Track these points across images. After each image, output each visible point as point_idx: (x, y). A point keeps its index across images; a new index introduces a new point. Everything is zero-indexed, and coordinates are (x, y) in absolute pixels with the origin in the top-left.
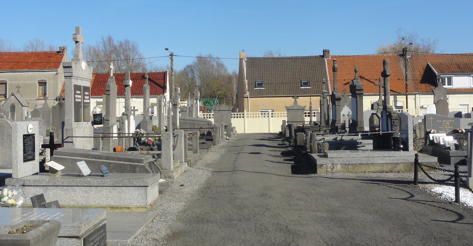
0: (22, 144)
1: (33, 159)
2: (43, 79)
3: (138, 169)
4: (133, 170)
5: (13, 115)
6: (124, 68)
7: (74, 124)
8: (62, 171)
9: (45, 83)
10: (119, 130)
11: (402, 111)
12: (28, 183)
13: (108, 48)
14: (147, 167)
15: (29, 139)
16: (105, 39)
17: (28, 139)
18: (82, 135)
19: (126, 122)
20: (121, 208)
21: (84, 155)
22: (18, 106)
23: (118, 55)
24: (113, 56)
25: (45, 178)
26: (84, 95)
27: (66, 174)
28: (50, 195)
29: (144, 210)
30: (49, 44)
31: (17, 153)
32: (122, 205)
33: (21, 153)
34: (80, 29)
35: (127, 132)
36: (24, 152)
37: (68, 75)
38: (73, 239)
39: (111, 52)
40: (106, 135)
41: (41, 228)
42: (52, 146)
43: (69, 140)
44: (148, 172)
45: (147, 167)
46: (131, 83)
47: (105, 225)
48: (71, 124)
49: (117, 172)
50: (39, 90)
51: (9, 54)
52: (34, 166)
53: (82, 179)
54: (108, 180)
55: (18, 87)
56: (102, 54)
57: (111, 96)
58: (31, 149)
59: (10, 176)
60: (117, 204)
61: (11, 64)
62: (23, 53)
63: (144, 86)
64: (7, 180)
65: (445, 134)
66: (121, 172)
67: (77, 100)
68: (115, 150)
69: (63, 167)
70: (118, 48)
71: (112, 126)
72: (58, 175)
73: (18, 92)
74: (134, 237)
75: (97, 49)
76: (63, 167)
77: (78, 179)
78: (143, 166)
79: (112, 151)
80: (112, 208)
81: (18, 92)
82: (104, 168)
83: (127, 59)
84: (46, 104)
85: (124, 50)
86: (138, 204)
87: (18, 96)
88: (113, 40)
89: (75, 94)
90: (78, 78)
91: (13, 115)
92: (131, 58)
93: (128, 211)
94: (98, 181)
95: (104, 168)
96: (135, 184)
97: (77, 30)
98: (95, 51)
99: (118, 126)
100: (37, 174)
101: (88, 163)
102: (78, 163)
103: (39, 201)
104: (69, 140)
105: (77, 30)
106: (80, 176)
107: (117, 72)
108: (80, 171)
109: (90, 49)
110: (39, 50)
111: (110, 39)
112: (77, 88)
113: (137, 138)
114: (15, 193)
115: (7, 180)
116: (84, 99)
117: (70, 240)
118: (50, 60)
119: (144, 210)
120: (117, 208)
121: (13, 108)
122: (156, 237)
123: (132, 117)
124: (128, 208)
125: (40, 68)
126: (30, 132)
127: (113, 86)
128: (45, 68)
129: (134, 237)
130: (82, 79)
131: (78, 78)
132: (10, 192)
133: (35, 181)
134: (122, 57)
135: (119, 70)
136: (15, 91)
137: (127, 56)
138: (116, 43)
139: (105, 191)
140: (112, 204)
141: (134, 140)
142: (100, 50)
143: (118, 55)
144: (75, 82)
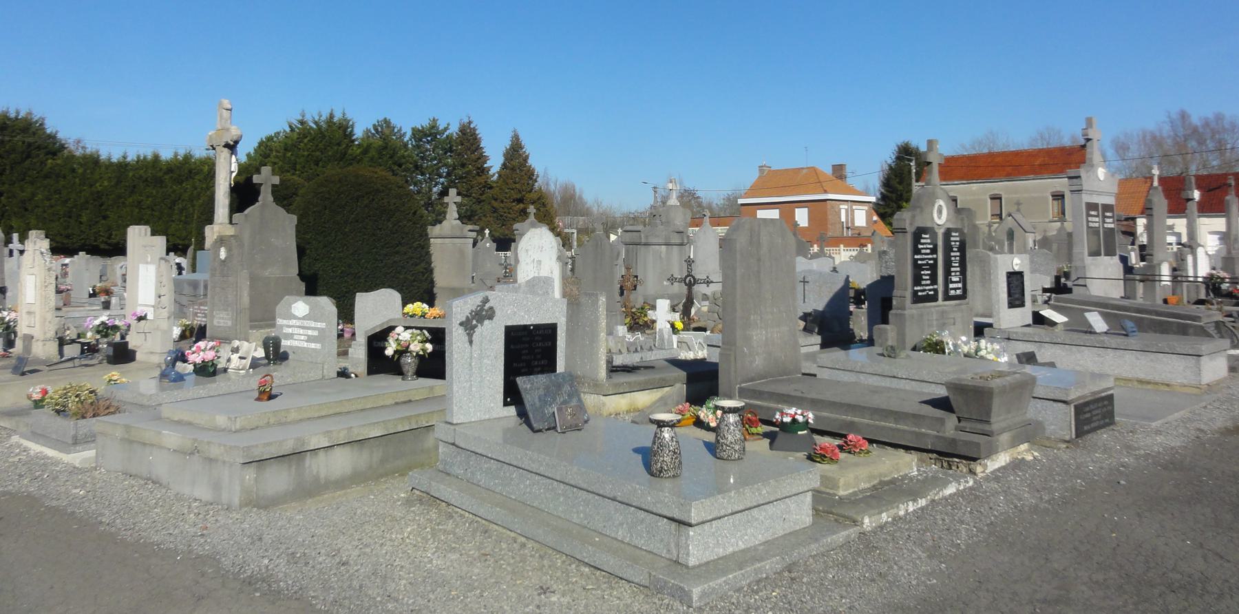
0: (1005, 285)
1: (1022, 305)
2: (1059, 189)
3: (1191, 331)
4: (1183, 330)
5: (1011, 245)
6: (1215, 163)
7: (1089, 260)
8: (1065, 324)
9: (1063, 196)
10: (1174, 270)
11: (608, 255)
12: (1014, 336)
13: (1181, 132)
14: (1212, 330)
15: (1015, 279)
16: (1174, 116)
17: (1014, 278)
18: (1103, 277)
19: (1190, 259)
20: (1157, 384)
21: (1102, 305)
22: (1018, 233)
23: (1201, 142)
24: (1193, 144)
25: (1040, 331)
26: (1105, 217)
27: (1068, 327)
28: (1044, 354)
29: (1196, 391)
30: (1068, 135)
31: (998, 295)
32: (1157, 379)
33: (1004, 296)
34: (1094, 120)
35: (1191, 273)
36: (1010, 294)
37: (1074, 188)
38: (1060, 404)
39: (1186, 138)
40: (1150, 277)
41: (1008, 378)
42: (1059, 288)
43: (1080, 282)
44: (1209, 335)
45: (1212, 330)
46: (1197, 195)
47: (1112, 396)
48: (1083, 260)
49: (1155, 332)
50: (1052, 207)
51: (1003, 154)
52: (1023, 316)
53: (1092, 337)
54: (1132, 341)
55: (1018, 204)
56: (1169, 141)
57: (1155, 217)
58: (1018, 291)
59: (990, 325)
60: (1149, 378)
61: (1009, 169)
62: (1026, 151)
63: (1227, 198)
64: (986, 330)
65: (434, 231)
66: (1162, 333)
67: (1091, 225)
68: (1165, 301)
69: (1065, 319)
70: (1201, 130)
71: (1159, 265)
72: (1058, 329)
73: (1018, 210)
74: (1165, 420)
75: (1158, 134)
76: (1065, 319)
77: (1087, 337)
78: (1202, 327)
79: (1160, 302)
80: (1141, 382)
81: (1018, 210)
82: (1129, 325)
83: (1220, 149)
84: (1062, 229)
85: (1214, 132)
86: (1185, 382)
87: (1018, 217)
88: (1189, 117)
89: (1088, 215)
90: (1092, 192)
91: (1011, 245)
92: (1229, 146)
93: (1167, 389)
94: (1119, 341)
95: (1129, 325)
96: (1179, 350)
97: (1089, 122)
98: (1154, 138)
99: (1170, 264)
100: (1028, 326)
101: (1105, 316)
102: (1087, 314)
103: (1029, 358)
104: (1080, 282)
105: (1089, 122)
106: (1091, 333)
107: (1200, 173)
108: (1090, 326)
109: (1144, 137)
110: (1054, 144)
111: (1184, 116)
112: (1091, 206)
113: (1212, 284)
114: (997, 346)
115: (986, 330)
116: (1104, 222)
117: (1055, 404)
118: (1067, 159)
119: (1196, 391)
120: (1149, 383)
121: (1011, 235)
122: (1202, 427)
123: (1200, 251)
124: (1168, 385)
125: (1053, 172)
126: (1017, 269)
127: (1160, 202)
128: (991, 177)
129: (1165, 420)
130: (1100, 193)
131: (1092, 192)
132: (989, 345)
133: (1025, 334)
134: (1211, 145)
135: (1204, 167)
136: (1013, 209)
137: (1220, 141)
138: (1195, 120)
139: (1129, 356)
140: (1142, 376)
141: (1207, 288)
142: (1165, 135)
143: (1201, 142)
144: (1086, 198)
